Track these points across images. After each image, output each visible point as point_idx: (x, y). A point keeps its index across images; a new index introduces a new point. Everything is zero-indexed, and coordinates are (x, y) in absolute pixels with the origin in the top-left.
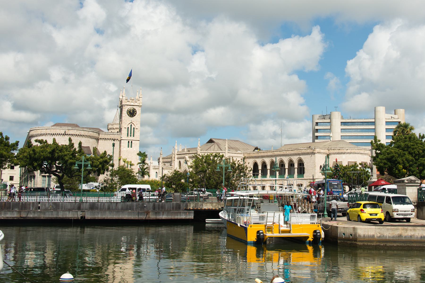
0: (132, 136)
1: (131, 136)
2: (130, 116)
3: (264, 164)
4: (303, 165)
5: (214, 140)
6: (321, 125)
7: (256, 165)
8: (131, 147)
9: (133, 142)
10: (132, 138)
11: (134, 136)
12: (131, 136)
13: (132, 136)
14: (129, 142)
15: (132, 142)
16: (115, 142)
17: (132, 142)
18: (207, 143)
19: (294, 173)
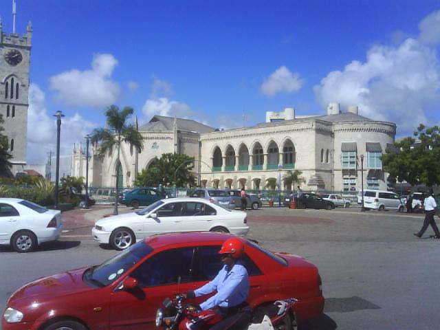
0: (14, 97)
1: (12, 97)
2: (11, 64)
3: (274, 147)
4: (247, 256)
5: (158, 118)
6: (5, 237)
7: (217, 151)
8: (13, 115)
9: (16, 107)
10: (14, 100)
11: (17, 97)
12: (12, 97)
13: (14, 97)
14: (8, 107)
15: (14, 108)
16: (355, 159)
17: (14, 108)
18: (150, 122)
19: (249, 164)
